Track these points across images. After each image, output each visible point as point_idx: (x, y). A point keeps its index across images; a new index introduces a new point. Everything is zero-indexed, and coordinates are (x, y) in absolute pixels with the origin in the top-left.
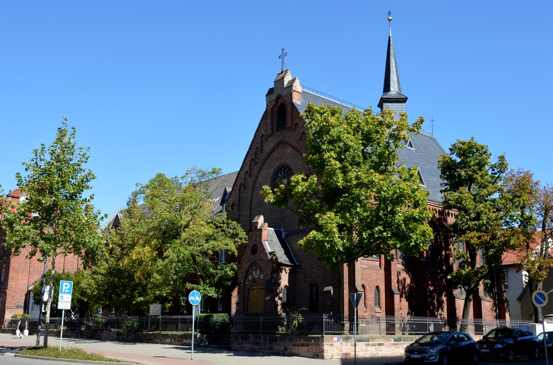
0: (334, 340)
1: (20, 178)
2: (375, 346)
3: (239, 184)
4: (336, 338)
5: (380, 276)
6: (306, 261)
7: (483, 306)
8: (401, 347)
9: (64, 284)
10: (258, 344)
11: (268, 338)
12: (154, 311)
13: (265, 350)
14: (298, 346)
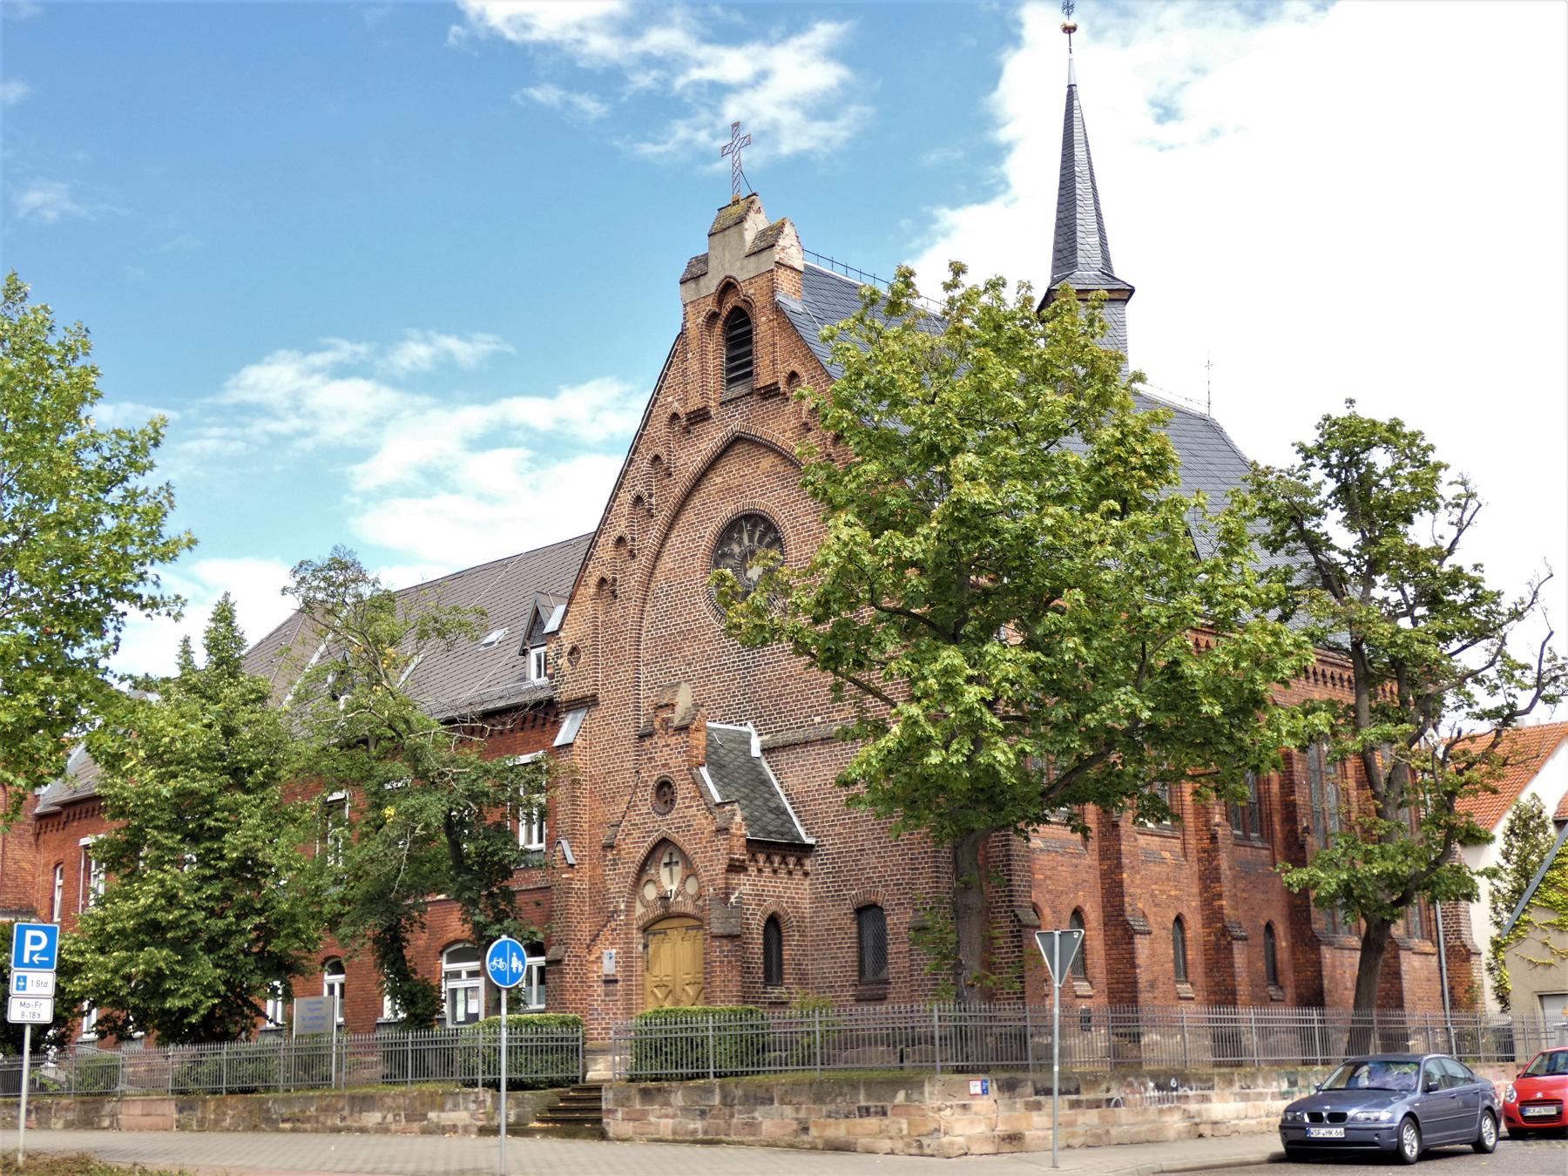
0: (972, 1092)
2: (1098, 1107)
3: (593, 581)
4: (979, 1083)
5: (1085, 876)
7: (1404, 967)
8: (1178, 1108)
11: (739, 1092)
12: (311, 1019)
14: (847, 1117)
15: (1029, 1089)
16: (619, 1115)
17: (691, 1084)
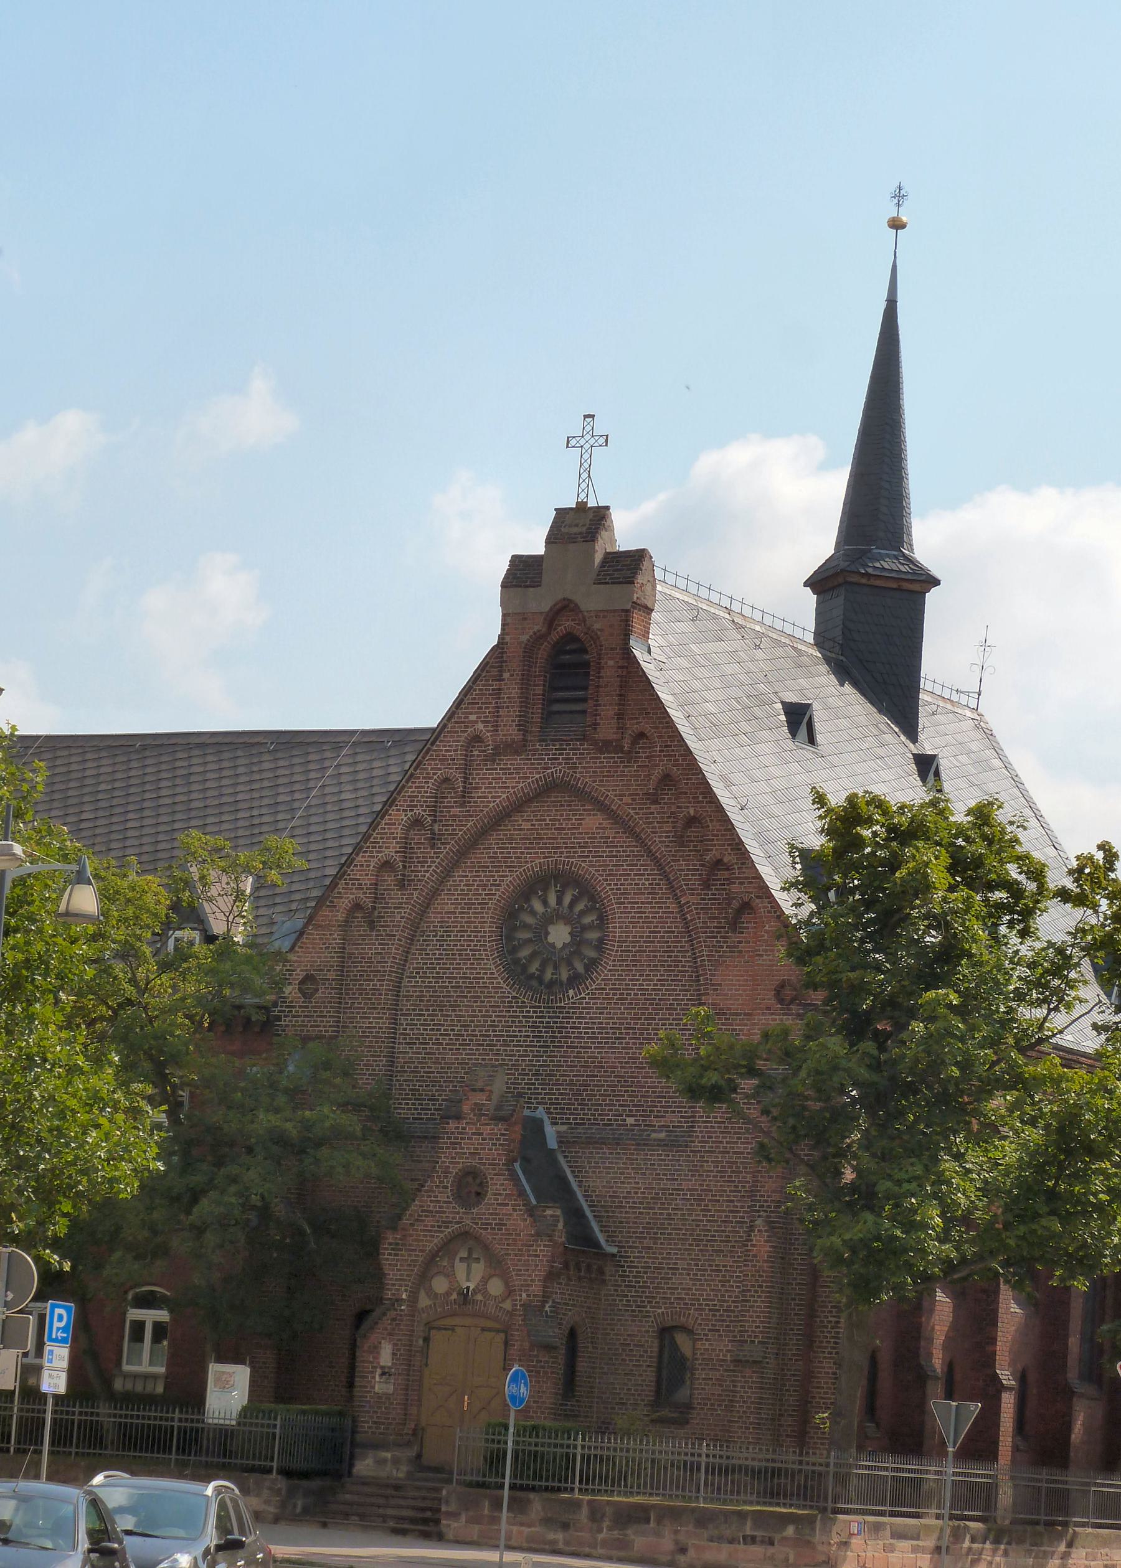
1: (161, 1042)
3: (344, 903)
6: (647, 1242)
9: (58, 1311)
10: (565, 1526)
13: (595, 1547)
14: (730, 1543)
15: (888, 1533)
16: (463, 1518)
17: (553, 1496)
